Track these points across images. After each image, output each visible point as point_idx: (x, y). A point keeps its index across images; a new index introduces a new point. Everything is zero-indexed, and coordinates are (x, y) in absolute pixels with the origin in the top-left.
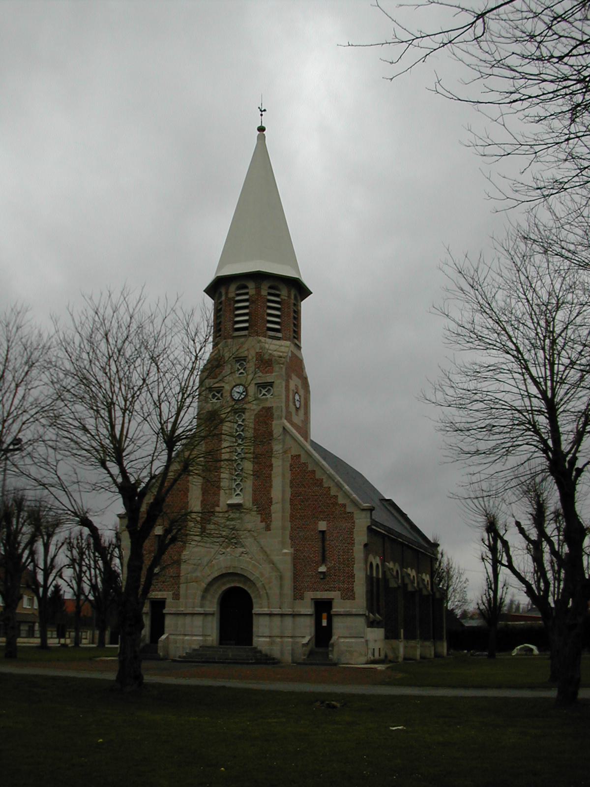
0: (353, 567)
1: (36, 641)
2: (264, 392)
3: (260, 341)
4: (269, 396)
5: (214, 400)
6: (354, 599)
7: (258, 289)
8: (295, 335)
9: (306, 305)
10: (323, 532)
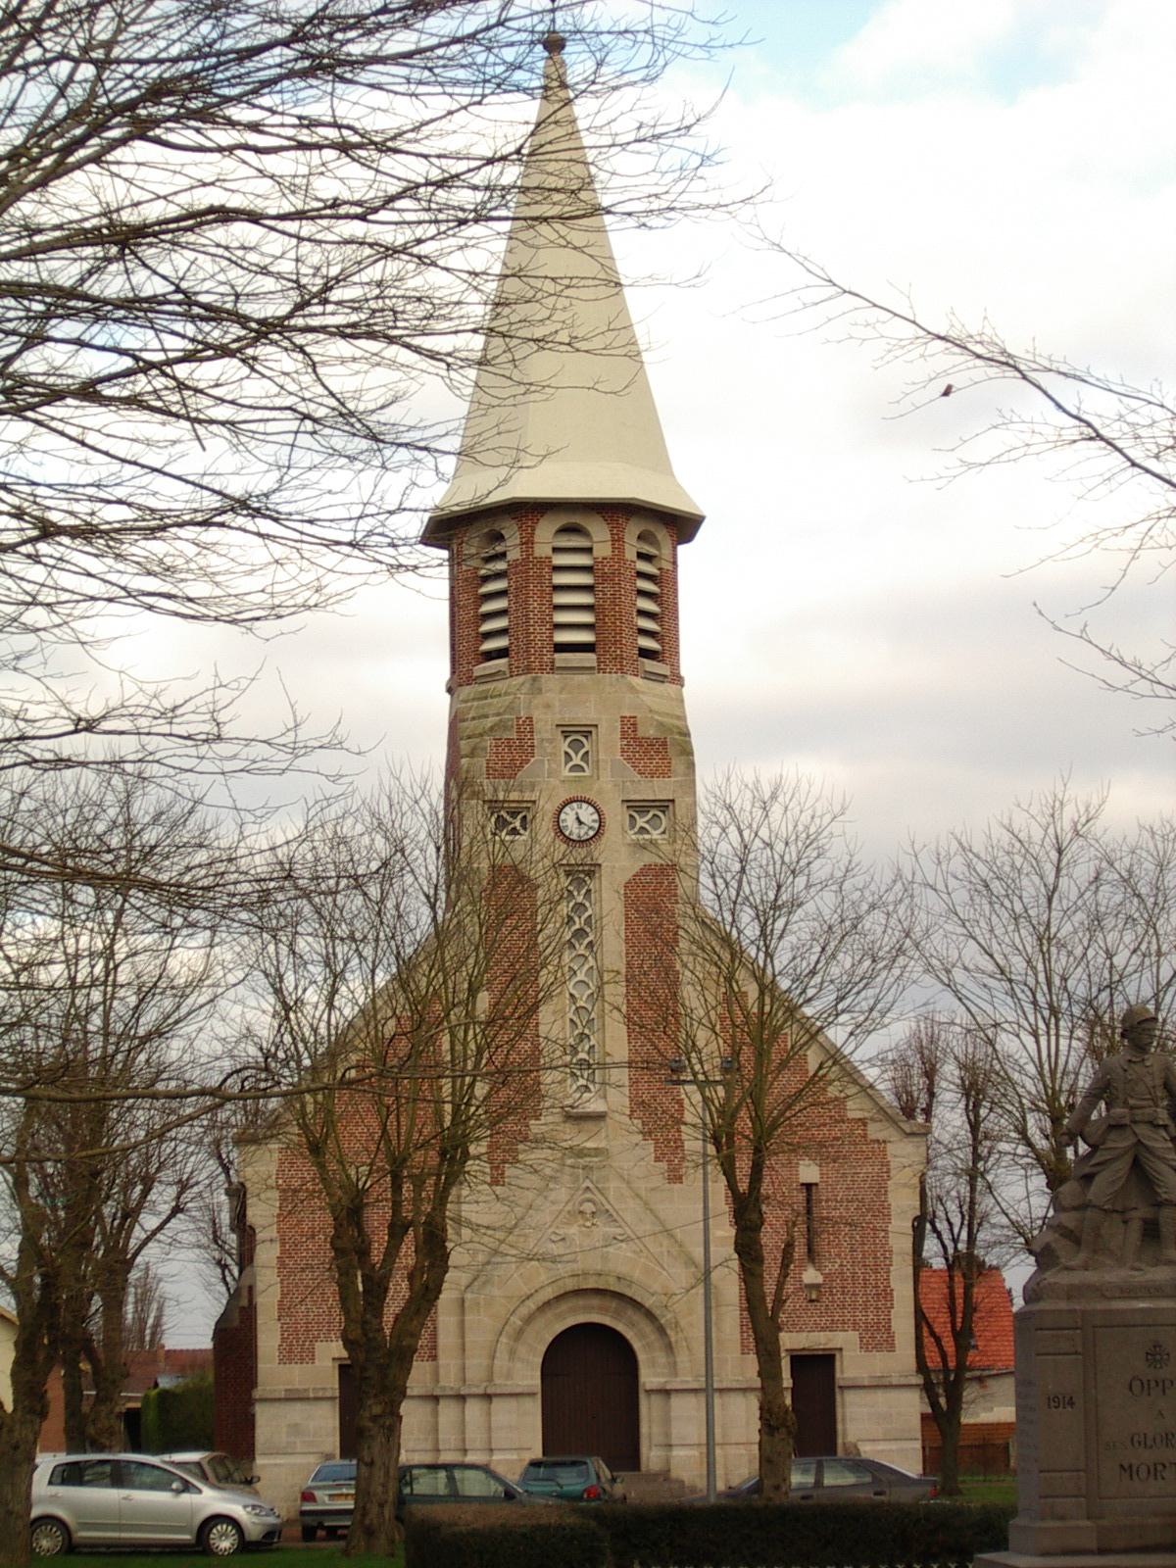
0: (888, 1272)
2: (641, 822)
3: (632, 689)
7: (617, 541)
10: (808, 1187)
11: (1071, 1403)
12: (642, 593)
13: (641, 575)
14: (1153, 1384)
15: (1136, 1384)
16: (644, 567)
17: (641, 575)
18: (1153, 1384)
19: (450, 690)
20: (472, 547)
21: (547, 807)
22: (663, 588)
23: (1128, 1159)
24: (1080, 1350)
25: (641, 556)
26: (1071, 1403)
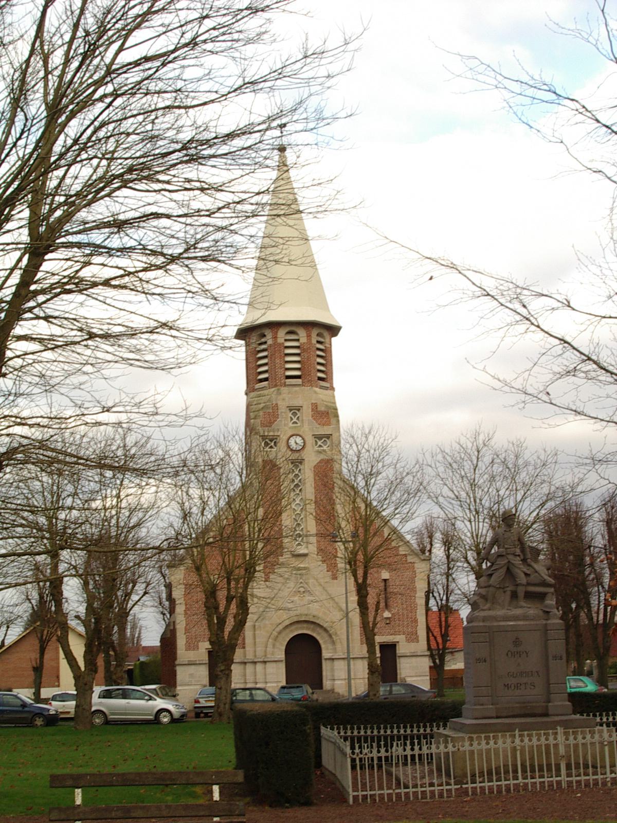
1: (351, 544)
2: (319, 443)
3: (315, 392)
4: (325, 448)
5: (267, 449)
6: (418, 642)
7: (309, 336)
8: (325, 378)
9: (337, 344)
10: (385, 580)
11: (485, 661)
15: (510, 653)
19: (246, 394)
20: (254, 338)
21: (284, 438)
23: (505, 568)
25: (318, 342)
26: (485, 661)
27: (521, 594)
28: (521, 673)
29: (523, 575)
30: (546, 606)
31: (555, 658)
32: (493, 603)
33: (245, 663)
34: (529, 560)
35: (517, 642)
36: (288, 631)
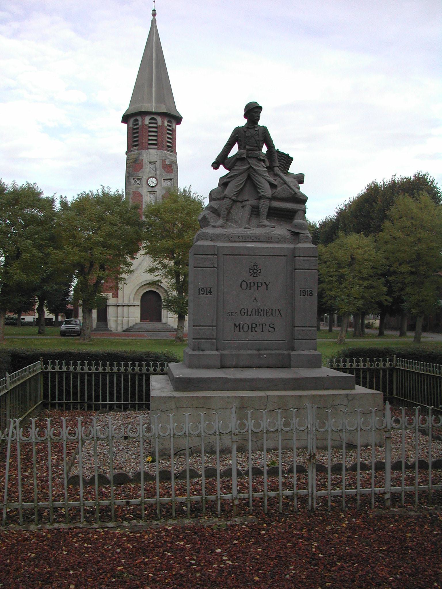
8: (171, 147)
11: (211, 292)
12: (168, 133)
13: (168, 130)
14: (252, 284)
15: (244, 284)
16: (168, 128)
17: (168, 130)
18: (252, 284)
19: (126, 154)
20: (131, 121)
21: (145, 177)
22: (173, 133)
23: (245, 176)
24: (216, 266)
25: (168, 125)
26: (211, 292)
27: (264, 211)
28: (258, 312)
29: (267, 186)
30: (296, 226)
31: (303, 292)
32: (227, 220)
33: (118, 306)
34: (276, 169)
35: (254, 270)
36: (142, 289)
